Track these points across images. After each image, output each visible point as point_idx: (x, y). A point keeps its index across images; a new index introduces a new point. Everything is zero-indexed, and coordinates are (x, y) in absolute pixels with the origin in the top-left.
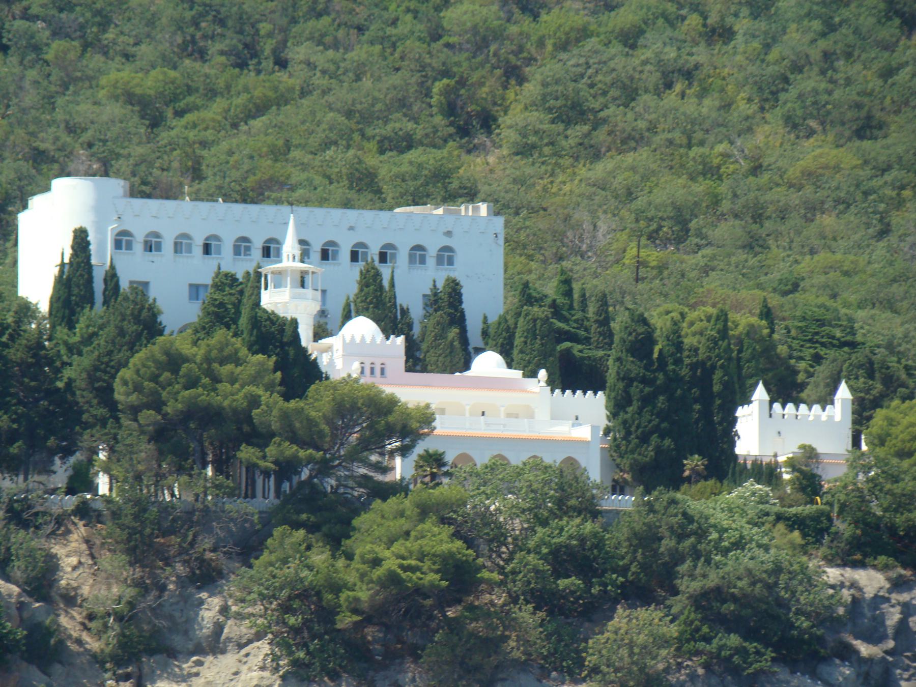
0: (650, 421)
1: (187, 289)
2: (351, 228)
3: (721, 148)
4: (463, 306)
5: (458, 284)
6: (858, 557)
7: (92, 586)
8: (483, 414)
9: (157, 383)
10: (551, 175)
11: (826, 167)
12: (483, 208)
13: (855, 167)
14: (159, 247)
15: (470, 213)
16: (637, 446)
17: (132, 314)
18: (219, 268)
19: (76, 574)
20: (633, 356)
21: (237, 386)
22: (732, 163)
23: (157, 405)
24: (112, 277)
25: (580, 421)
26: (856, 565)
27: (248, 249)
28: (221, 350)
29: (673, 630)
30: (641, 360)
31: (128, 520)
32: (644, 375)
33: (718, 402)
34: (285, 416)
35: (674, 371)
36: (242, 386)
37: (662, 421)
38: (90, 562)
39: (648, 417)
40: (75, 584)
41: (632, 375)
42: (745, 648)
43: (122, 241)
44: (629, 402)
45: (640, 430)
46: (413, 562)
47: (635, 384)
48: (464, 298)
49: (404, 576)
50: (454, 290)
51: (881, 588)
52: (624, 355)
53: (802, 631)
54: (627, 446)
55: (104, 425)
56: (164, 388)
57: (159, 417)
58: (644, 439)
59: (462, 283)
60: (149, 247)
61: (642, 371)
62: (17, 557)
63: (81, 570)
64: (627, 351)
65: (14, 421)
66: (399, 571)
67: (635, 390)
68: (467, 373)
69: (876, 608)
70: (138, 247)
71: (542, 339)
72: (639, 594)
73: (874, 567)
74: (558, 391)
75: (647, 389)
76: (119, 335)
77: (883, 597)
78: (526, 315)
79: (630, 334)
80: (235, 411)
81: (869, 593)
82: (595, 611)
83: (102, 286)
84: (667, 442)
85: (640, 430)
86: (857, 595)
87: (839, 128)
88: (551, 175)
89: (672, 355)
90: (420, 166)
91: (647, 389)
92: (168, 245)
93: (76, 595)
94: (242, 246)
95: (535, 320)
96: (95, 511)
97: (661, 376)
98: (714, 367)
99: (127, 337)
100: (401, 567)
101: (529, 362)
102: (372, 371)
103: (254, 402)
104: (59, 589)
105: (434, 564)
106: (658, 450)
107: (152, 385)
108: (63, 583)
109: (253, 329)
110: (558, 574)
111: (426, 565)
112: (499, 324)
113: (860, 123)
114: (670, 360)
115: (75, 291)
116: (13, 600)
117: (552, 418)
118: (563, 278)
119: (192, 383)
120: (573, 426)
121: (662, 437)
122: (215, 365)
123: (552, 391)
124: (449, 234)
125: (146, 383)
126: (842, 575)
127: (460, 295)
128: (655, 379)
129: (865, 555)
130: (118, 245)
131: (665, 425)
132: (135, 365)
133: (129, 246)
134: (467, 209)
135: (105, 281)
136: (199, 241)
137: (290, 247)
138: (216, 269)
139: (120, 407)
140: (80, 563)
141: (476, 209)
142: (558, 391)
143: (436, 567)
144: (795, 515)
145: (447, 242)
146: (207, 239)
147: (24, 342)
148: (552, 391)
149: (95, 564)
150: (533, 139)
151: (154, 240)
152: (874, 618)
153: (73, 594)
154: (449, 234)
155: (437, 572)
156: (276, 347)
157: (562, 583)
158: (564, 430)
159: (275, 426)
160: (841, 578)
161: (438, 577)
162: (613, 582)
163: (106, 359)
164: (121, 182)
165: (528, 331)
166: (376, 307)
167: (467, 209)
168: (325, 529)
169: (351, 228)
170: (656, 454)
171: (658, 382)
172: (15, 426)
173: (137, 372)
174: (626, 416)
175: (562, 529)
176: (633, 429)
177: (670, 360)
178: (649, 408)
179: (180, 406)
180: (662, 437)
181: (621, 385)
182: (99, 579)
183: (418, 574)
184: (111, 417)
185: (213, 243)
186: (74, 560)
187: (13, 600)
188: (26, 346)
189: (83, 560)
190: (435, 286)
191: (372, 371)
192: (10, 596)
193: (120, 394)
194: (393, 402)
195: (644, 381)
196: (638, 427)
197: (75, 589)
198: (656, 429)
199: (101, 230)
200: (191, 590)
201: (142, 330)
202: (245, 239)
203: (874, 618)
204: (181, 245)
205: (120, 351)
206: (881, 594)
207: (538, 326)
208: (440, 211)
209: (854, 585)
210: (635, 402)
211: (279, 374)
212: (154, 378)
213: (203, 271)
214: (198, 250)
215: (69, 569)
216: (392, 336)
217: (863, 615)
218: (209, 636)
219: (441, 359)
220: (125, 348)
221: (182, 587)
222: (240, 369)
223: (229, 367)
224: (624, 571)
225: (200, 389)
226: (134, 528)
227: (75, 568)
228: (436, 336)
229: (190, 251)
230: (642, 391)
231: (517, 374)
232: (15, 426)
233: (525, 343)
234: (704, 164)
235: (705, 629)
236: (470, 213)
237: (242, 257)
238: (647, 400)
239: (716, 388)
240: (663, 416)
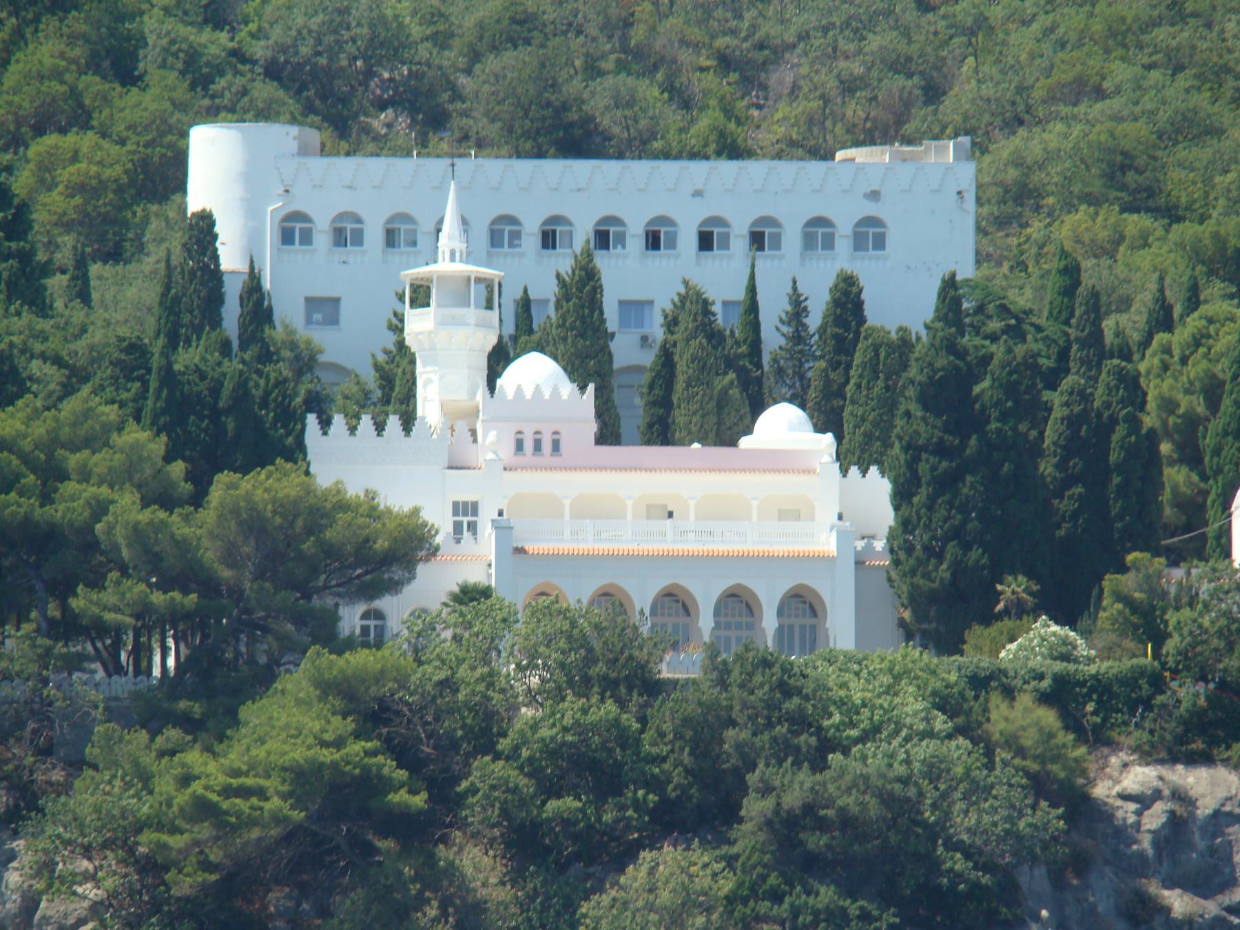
2: (698, 193)
6: (1198, 745)
8: (670, 515)
14: (358, 238)
26: (1192, 760)
28: (75, 424)
29: (727, 885)
30: (938, 415)
33: (1116, 480)
35: (999, 431)
42: (844, 910)
43: (293, 230)
51: (1230, 799)
53: (958, 877)
61: (938, 433)
69: (1218, 832)
70: (322, 240)
72: (673, 821)
73: (1226, 762)
74: (854, 470)
77: (1230, 814)
81: (1205, 808)
82: (608, 853)
86: (1180, 810)
98: (1114, 421)
101: (863, 420)
102: (538, 445)
103: (100, 509)
106: (957, 569)
110: (552, 790)
114: (995, 414)
115: (186, 319)
124: (874, 195)
126: (1161, 778)
129: (1214, 742)
130: (287, 237)
133: (307, 238)
142: (854, 470)
144: (1095, 677)
145: (871, 209)
146: (391, 220)
148: (844, 472)
152: (1212, 851)
157: (553, 805)
160: (1157, 784)
162: (637, 805)
166: (582, 335)
169: (698, 193)
170: (954, 575)
171: (968, 452)
177: (995, 414)
178: (947, 497)
190: (795, 289)
191: (538, 445)
195: (941, 450)
199: (251, 208)
202: (512, 220)
203: (1212, 851)
206: (1228, 808)
209: (1179, 796)
217: (1191, 846)
218: (15, 916)
224: (654, 784)
235: (773, 880)
239: (1114, 457)
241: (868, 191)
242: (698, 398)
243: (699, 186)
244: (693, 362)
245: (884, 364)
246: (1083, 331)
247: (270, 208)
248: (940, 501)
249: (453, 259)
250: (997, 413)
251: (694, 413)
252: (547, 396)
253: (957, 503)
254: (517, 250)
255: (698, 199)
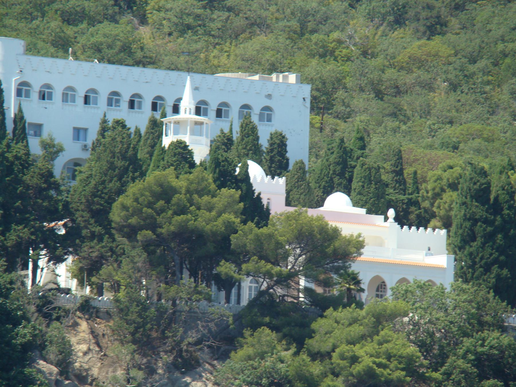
0: (491, 255)
1: (71, 132)
3: (335, 35)
4: (288, 155)
5: (284, 137)
7: (100, 368)
9: (152, 209)
10: (206, 51)
11: (429, 54)
12: (292, 78)
13: (449, 56)
15: (281, 80)
16: (482, 274)
17: (120, 152)
18: (105, 116)
19: (87, 358)
20: (477, 201)
21: (214, 213)
22: (344, 48)
23: (153, 226)
24: (19, 118)
25: (432, 251)
27: (118, 101)
31: (133, 317)
32: (486, 217)
34: (258, 239)
35: (509, 215)
36: (219, 214)
37: (500, 255)
38: (97, 349)
39: (489, 250)
40: (86, 367)
41: (477, 217)
44: (473, 238)
45: (483, 262)
46: (384, 361)
47: (479, 224)
48: (288, 149)
49: (379, 371)
50: (282, 142)
52: (468, 200)
54: (473, 274)
55: (101, 240)
56: (159, 214)
57: (155, 236)
58: (487, 269)
59: (287, 136)
60: (43, 96)
61: (484, 213)
62: (51, 342)
63: (90, 355)
64: (472, 197)
65: (32, 234)
66: (375, 367)
67: (479, 228)
68: (321, 209)
71: (376, 184)
75: (489, 229)
76: (110, 168)
78: (363, 165)
79: (475, 184)
80: (214, 234)
83: (238, 130)
84: (505, 272)
85: (483, 262)
87: (414, 25)
88: (206, 51)
89: (507, 202)
90: (116, 38)
91: (489, 229)
92: (57, 95)
93: (87, 375)
94: (114, 98)
95: (370, 169)
96: (94, 308)
97: (499, 218)
99: (117, 171)
100: (374, 363)
104: (73, 369)
105: (400, 363)
106: (498, 277)
107: (150, 211)
108: (77, 365)
109: (215, 168)
111: (394, 364)
112: (322, 170)
113: (432, 20)
116: (53, 378)
117: (398, 247)
118: (359, 136)
119: (182, 211)
120: (426, 255)
121: (501, 267)
122: (196, 196)
123: (402, 227)
124: (269, 96)
125: (145, 209)
127: (286, 145)
128: (495, 220)
131: (502, 258)
132: (134, 194)
133: (27, 95)
134: (278, 77)
135: (15, 121)
136: (81, 94)
137: (187, 104)
138: (102, 117)
139: (113, 225)
140: (89, 349)
141: (285, 78)
143: (402, 366)
145: (267, 103)
147: (37, 171)
149: (101, 350)
150: (190, 20)
151: (47, 90)
153: (85, 374)
154: (269, 96)
155: (403, 369)
156: (232, 183)
158: (418, 257)
159: (250, 247)
161: (404, 373)
163: (100, 188)
164: (22, 42)
165: (365, 177)
167: (278, 77)
168: (286, 330)
170: (496, 280)
171: (497, 223)
172: (33, 237)
173: (136, 200)
174: (471, 250)
175: (484, 340)
176: (477, 260)
178: (491, 243)
179: (172, 228)
180: (501, 267)
181: (468, 224)
182: (106, 363)
183: (388, 370)
184: (106, 233)
185: (92, 95)
186: (84, 347)
187: (53, 378)
188: (39, 174)
189: (91, 347)
192: (51, 374)
193: (116, 215)
194: (336, 232)
195: (486, 221)
196: (482, 258)
197: (87, 370)
198: (496, 261)
200: (177, 374)
201: (129, 165)
204: (68, 95)
205: (111, 181)
207: (373, 174)
208: (256, 77)
210: (478, 239)
211: (242, 205)
212: (150, 205)
213: (91, 119)
214: (80, 101)
215: (81, 354)
216: (276, 177)
219: (302, 196)
220: (115, 179)
221: (169, 372)
222: (215, 199)
223: (206, 198)
225: (190, 215)
226: (138, 323)
227: (85, 354)
228: (298, 178)
229: (74, 101)
230: (485, 230)
231: (363, 211)
232: (33, 237)
233: (363, 187)
234: (323, 47)
236: (281, 80)
237: (113, 107)
238: (489, 237)
240: (501, 250)
241: (267, 94)
242: (303, 187)
243: (198, 86)
244: (300, 169)
245: (374, 177)
246: (397, 167)
247: (14, 79)
248: (487, 245)
249: (190, 113)
250: (507, 206)
251: (301, 194)
252: (259, 181)
253: (495, 247)
254: (118, 108)
255: (197, 91)
